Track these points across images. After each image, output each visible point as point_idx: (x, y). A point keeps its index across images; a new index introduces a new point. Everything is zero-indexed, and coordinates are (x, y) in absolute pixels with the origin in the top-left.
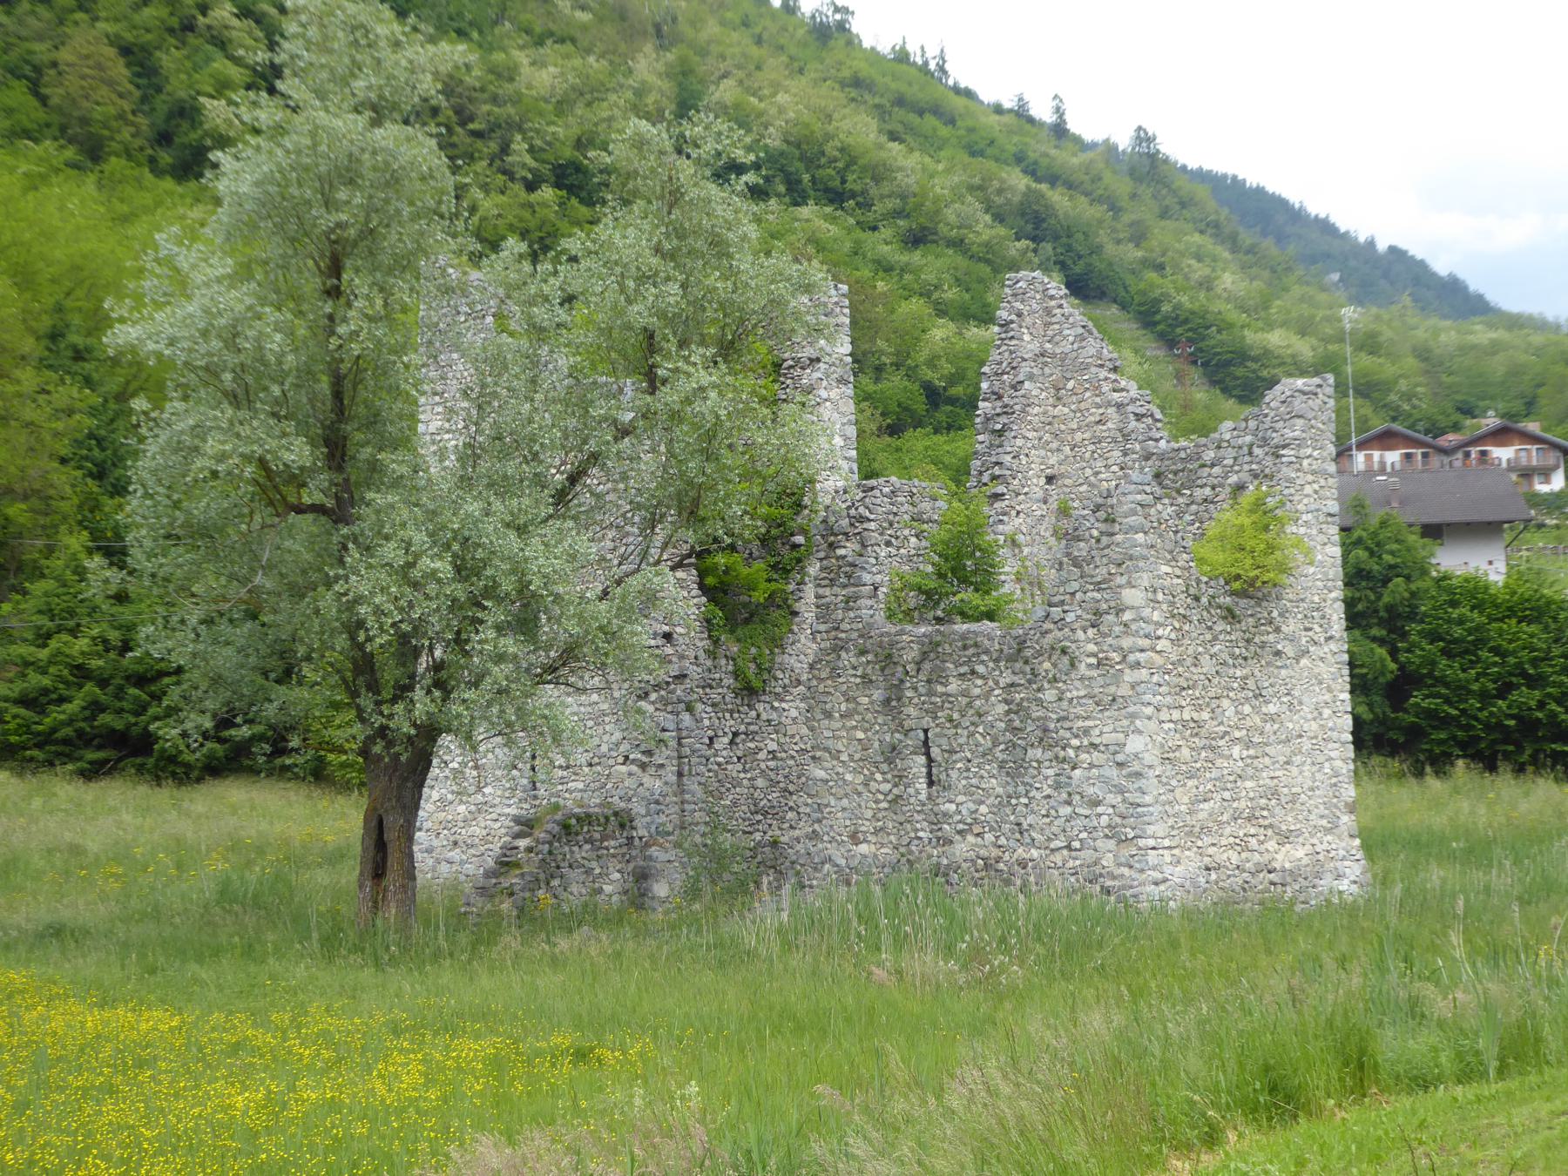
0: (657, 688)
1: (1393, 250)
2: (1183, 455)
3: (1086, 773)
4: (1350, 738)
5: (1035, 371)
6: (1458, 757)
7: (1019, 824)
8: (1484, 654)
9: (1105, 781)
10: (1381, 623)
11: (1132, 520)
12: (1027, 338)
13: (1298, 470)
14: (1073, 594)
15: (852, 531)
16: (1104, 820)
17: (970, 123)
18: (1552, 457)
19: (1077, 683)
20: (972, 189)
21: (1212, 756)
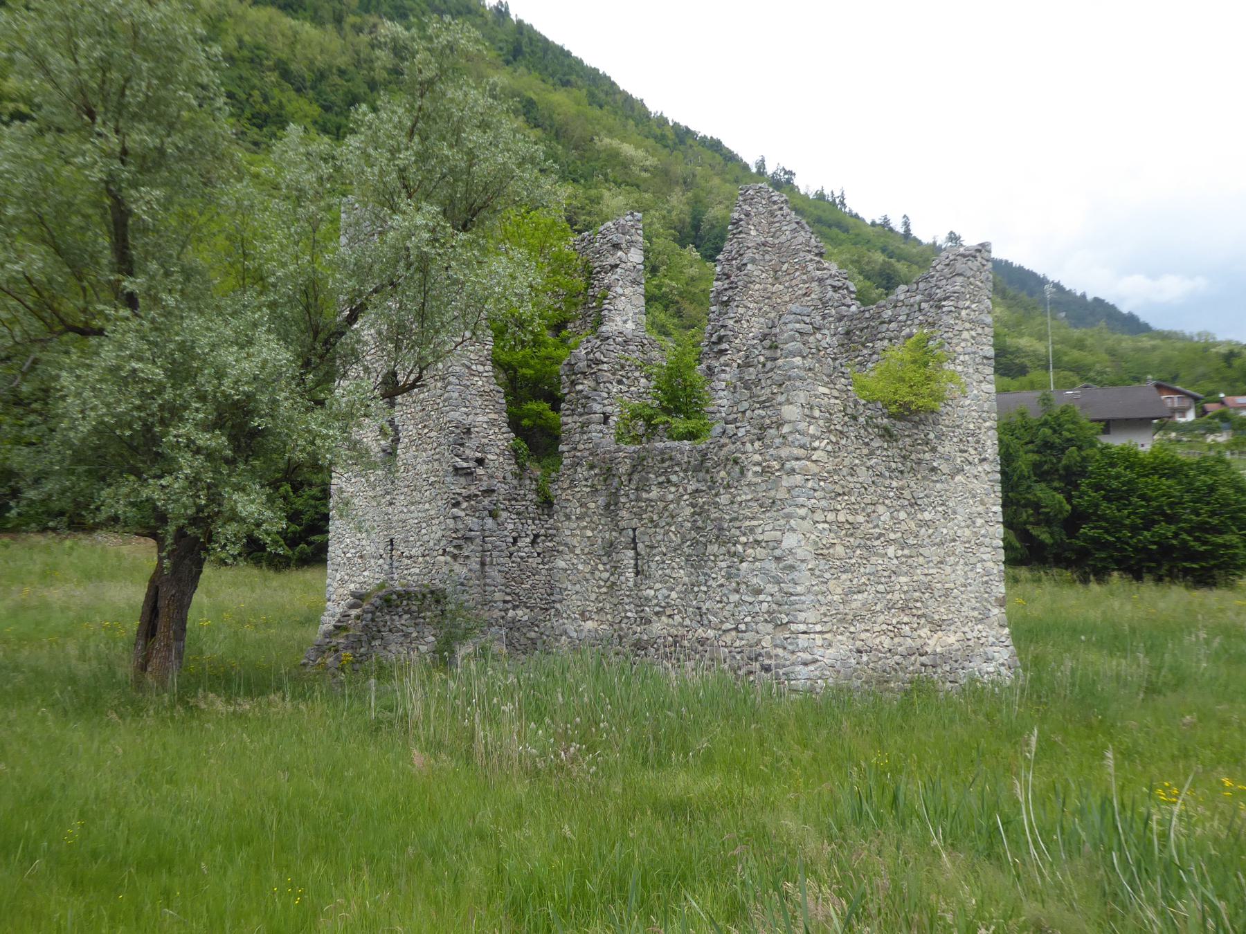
0: (468, 498)
1: (1096, 299)
2: (867, 315)
3: (751, 566)
4: (1001, 544)
5: (757, 256)
6: (1114, 570)
7: (699, 608)
8: (1134, 499)
9: (765, 572)
10: (1061, 478)
11: (791, 346)
12: (753, 233)
13: (956, 318)
14: (744, 412)
15: (589, 371)
16: (765, 606)
17: (857, 231)
18: (1187, 402)
19: (746, 489)
20: (852, 262)
21: (866, 554)
